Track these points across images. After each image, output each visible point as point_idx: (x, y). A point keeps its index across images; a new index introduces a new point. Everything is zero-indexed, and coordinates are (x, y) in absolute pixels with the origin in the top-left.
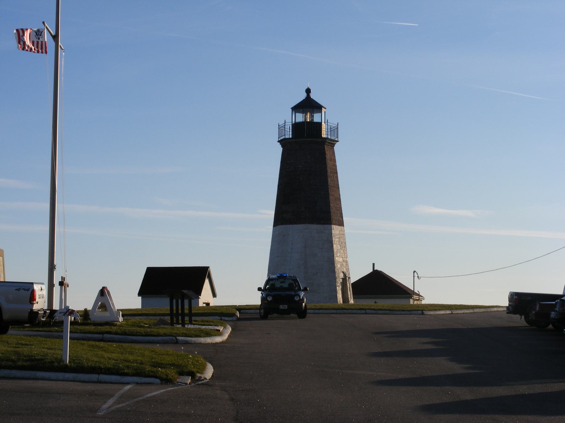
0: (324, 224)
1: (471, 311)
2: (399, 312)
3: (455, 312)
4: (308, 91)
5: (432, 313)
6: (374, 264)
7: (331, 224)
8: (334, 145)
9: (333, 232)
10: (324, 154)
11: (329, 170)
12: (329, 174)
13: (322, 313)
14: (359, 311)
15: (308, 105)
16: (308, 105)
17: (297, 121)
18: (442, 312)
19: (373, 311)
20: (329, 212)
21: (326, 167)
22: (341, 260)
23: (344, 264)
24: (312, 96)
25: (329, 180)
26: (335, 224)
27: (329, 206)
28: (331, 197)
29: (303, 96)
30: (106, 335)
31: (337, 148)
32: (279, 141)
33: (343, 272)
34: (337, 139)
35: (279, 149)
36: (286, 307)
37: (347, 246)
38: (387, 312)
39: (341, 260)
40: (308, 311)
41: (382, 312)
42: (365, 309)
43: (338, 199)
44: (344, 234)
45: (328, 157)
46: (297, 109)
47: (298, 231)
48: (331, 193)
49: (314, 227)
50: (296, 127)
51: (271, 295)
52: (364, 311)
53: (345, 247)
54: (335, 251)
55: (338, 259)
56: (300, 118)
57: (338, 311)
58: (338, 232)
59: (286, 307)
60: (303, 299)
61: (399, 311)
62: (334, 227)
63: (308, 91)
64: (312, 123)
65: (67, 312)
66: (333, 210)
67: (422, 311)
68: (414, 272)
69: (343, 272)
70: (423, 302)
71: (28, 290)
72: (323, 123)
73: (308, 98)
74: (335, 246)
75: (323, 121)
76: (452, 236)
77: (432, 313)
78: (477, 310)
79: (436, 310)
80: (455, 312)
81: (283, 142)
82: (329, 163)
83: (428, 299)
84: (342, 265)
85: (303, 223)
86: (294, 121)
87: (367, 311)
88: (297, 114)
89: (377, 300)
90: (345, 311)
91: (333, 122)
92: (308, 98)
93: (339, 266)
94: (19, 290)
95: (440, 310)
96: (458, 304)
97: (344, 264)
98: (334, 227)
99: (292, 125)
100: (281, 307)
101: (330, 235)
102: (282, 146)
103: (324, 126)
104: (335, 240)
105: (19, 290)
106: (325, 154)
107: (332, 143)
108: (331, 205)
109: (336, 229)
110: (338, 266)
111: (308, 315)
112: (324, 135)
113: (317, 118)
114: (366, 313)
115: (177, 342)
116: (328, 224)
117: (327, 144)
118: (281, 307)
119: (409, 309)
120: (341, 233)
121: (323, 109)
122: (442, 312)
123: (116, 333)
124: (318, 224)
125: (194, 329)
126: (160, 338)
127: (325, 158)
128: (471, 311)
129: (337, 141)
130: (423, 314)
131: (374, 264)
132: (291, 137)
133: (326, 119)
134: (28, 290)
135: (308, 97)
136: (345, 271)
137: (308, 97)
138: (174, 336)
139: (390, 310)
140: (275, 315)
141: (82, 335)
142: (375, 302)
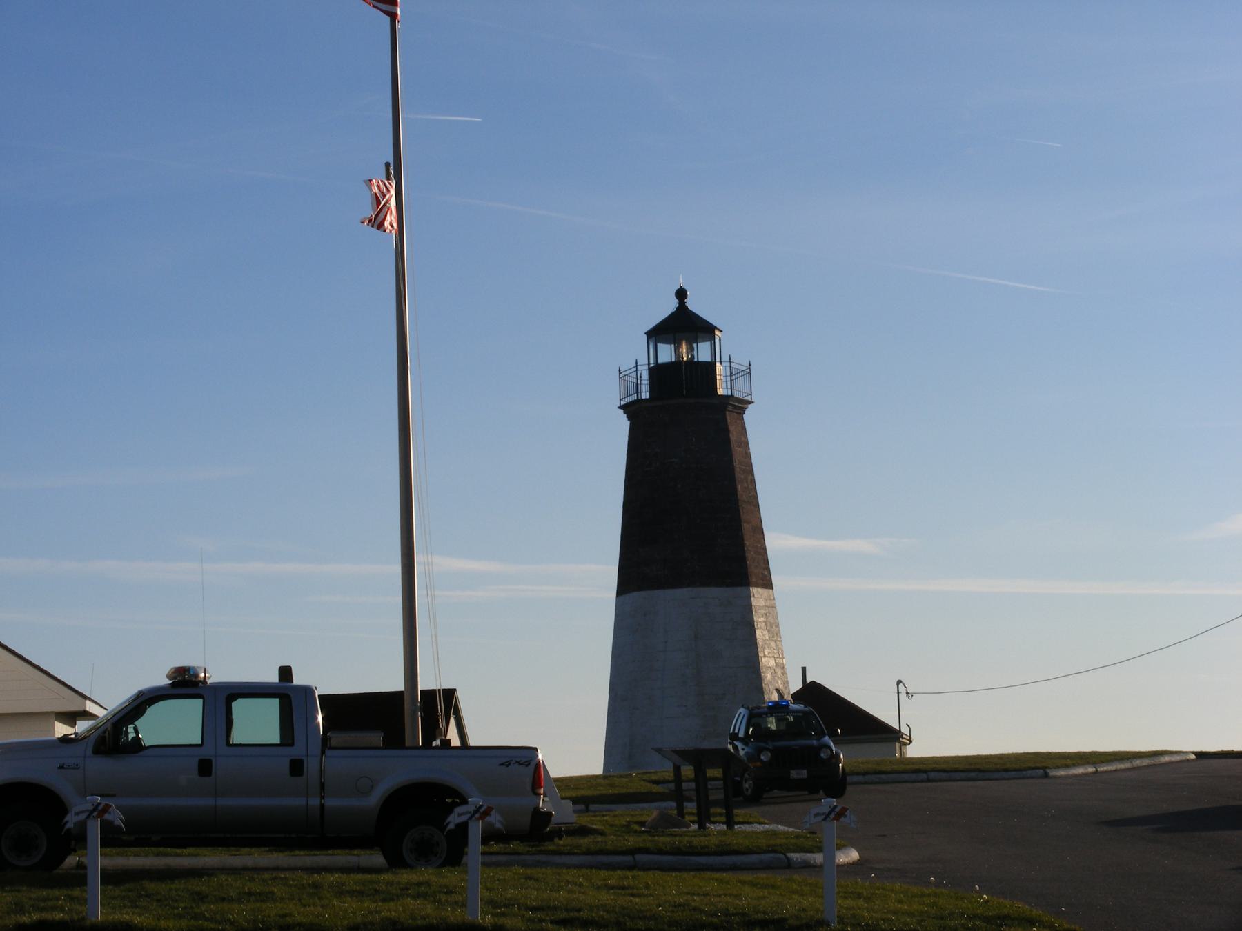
1: (1146, 762)
2: (996, 775)
3: (1102, 768)
4: (681, 294)
5: (1062, 773)
6: (804, 669)
8: (743, 409)
10: (726, 431)
11: (737, 466)
12: (739, 475)
13: (860, 783)
14: (913, 776)
15: (683, 325)
16: (683, 325)
17: (660, 361)
18: (1080, 771)
19: (944, 775)
20: (742, 559)
21: (731, 460)
22: (772, 663)
23: (779, 672)
24: (691, 304)
25: (739, 487)
26: (757, 586)
27: (743, 545)
28: (745, 526)
29: (671, 305)
30: (639, 857)
31: (749, 416)
32: (621, 407)
33: (777, 690)
34: (748, 398)
35: (622, 426)
36: (804, 774)
37: (782, 634)
38: (973, 774)
39: (772, 663)
40: (849, 778)
41: (963, 775)
42: (925, 771)
43: (759, 530)
44: (774, 607)
45: (733, 437)
46: (658, 334)
47: (675, 604)
48: (744, 516)
49: (714, 593)
50: (658, 373)
51: (767, 749)
52: (924, 776)
53: (778, 634)
54: (760, 643)
56: (666, 354)
57: (868, 778)
58: (762, 603)
59: (804, 774)
60: (837, 756)
61: (997, 771)
62: (754, 590)
63: (681, 294)
64: (693, 365)
65: (830, 813)
66: (750, 555)
67: (1044, 768)
68: (899, 682)
69: (777, 690)
71: (528, 764)
72: (718, 364)
73: (682, 309)
74: (758, 632)
75: (718, 359)
76: (977, 609)
77: (1062, 773)
78: (1137, 763)
79: (1067, 766)
80: (1102, 768)
82: (737, 450)
83: (924, 744)
84: (774, 674)
85: (688, 586)
86: (652, 361)
87: (932, 775)
88: (659, 345)
90: (883, 776)
91: (740, 362)
92: (682, 309)
93: (769, 676)
94: (507, 764)
95: (1074, 765)
96: (1021, 750)
97: (779, 672)
98: (755, 591)
99: (651, 370)
100: (794, 774)
101: (748, 608)
102: (629, 418)
104: (759, 620)
105: (507, 764)
106: (727, 431)
107: (739, 406)
108: (747, 543)
109: (758, 596)
110: (767, 676)
111: (849, 789)
112: (721, 392)
113: (703, 352)
114: (929, 780)
115: (789, 865)
116: (741, 585)
118: (794, 774)
120: (769, 603)
121: (717, 332)
122: (1080, 771)
123: (661, 852)
125: (784, 833)
126: (754, 858)
127: (727, 441)
128: (1146, 762)
129: (751, 403)
130: (1046, 775)
131: (804, 669)
132: (645, 395)
133: (732, 354)
134: (528, 764)
135: (682, 307)
136: (781, 686)
137: (682, 307)
140: (776, 792)
141: (589, 858)
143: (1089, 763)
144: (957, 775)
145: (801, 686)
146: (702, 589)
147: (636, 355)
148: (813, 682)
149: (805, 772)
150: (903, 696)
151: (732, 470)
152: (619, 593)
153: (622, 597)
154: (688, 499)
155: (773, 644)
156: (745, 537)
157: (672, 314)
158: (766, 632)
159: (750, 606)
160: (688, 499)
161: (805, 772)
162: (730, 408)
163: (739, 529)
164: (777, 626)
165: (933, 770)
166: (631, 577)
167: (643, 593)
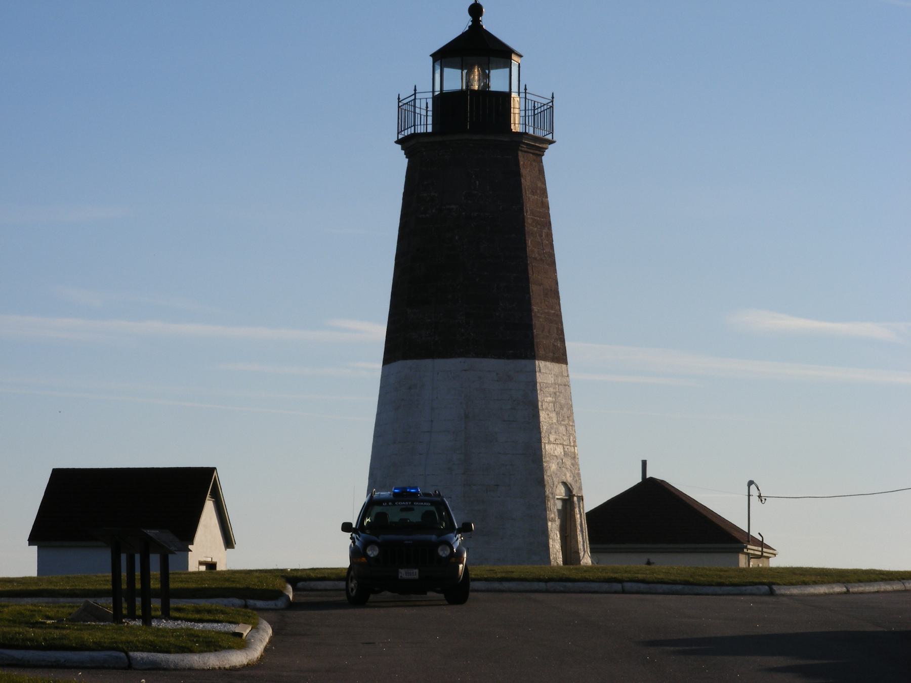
0: (516, 357)
1: (897, 586)
3: (856, 588)
4: (476, 11)
5: (795, 591)
6: (644, 463)
7: (533, 357)
9: (540, 378)
10: (516, 175)
11: (529, 218)
12: (530, 226)
13: (510, 591)
14: (605, 586)
15: (476, 47)
16: (476, 47)
18: (822, 589)
19: (642, 586)
21: (521, 210)
22: (559, 451)
23: (568, 462)
24: (487, 23)
25: (529, 242)
26: (545, 359)
27: (530, 310)
28: (534, 288)
29: (463, 23)
31: (549, 158)
32: (398, 142)
33: (565, 484)
34: (549, 137)
35: (398, 164)
36: (415, 574)
37: (576, 416)
38: (679, 587)
39: (559, 451)
40: (473, 585)
41: (666, 587)
43: (554, 293)
44: (567, 385)
45: (526, 182)
46: (445, 56)
47: (441, 374)
48: (533, 276)
50: (444, 103)
52: (618, 587)
53: (570, 417)
54: (544, 427)
55: (552, 449)
56: (454, 80)
57: (550, 585)
58: (550, 379)
59: (415, 574)
60: (459, 554)
62: (541, 365)
63: (476, 11)
64: (485, 93)
66: (538, 322)
67: (770, 585)
68: (751, 483)
69: (565, 484)
70: (774, 563)
74: (543, 415)
75: (515, 88)
77: (795, 591)
79: (805, 583)
81: (410, 144)
83: (783, 558)
85: (460, 355)
86: (438, 88)
87: (628, 586)
89: (653, 558)
90: (569, 584)
91: (540, 91)
97: (568, 462)
98: (541, 365)
99: (435, 99)
100: (403, 573)
101: (532, 385)
102: (408, 154)
103: (516, 101)
104: (545, 400)
106: (517, 175)
108: (535, 308)
109: (546, 372)
110: (551, 467)
111: (471, 595)
112: (517, 126)
113: (498, 81)
115: (129, 666)
116: (526, 357)
117: (524, 148)
118: (403, 573)
119: (736, 580)
120: (560, 380)
121: (514, 57)
122: (822, 589)
124: (499, 356)
126: (85, 655)
128: (897, 586)
129: (551, 142)
130: (772, 593)
131: (644, 463)
132: (430, 129)
133: (522, 84)
136: (569, 479)
138: (122, 650)
139: (687, 583)
140: (387, 594)
142: (649, 563)
143: (838, 582)
144: (660, 587)
145: (640, 480)
146: (477, 360)
147: (422, 80)
148: (651, 478)
149: (417, 571)
150: (754, 499)
151: (522, 221)
152: (386, 361)
153: (388, 366)
154: (472, 250)
155: (562, 429)
156: (533, 302)
157: (464, 35)
158: (553, 415)
159: (534, 383)
160: (472, 250)
161: (417, 571)
162: (524, 148)
163: (526, 290)
164: (570, 407)
165: (631, 580)
166: (399, 346)
167: (410, 363)
